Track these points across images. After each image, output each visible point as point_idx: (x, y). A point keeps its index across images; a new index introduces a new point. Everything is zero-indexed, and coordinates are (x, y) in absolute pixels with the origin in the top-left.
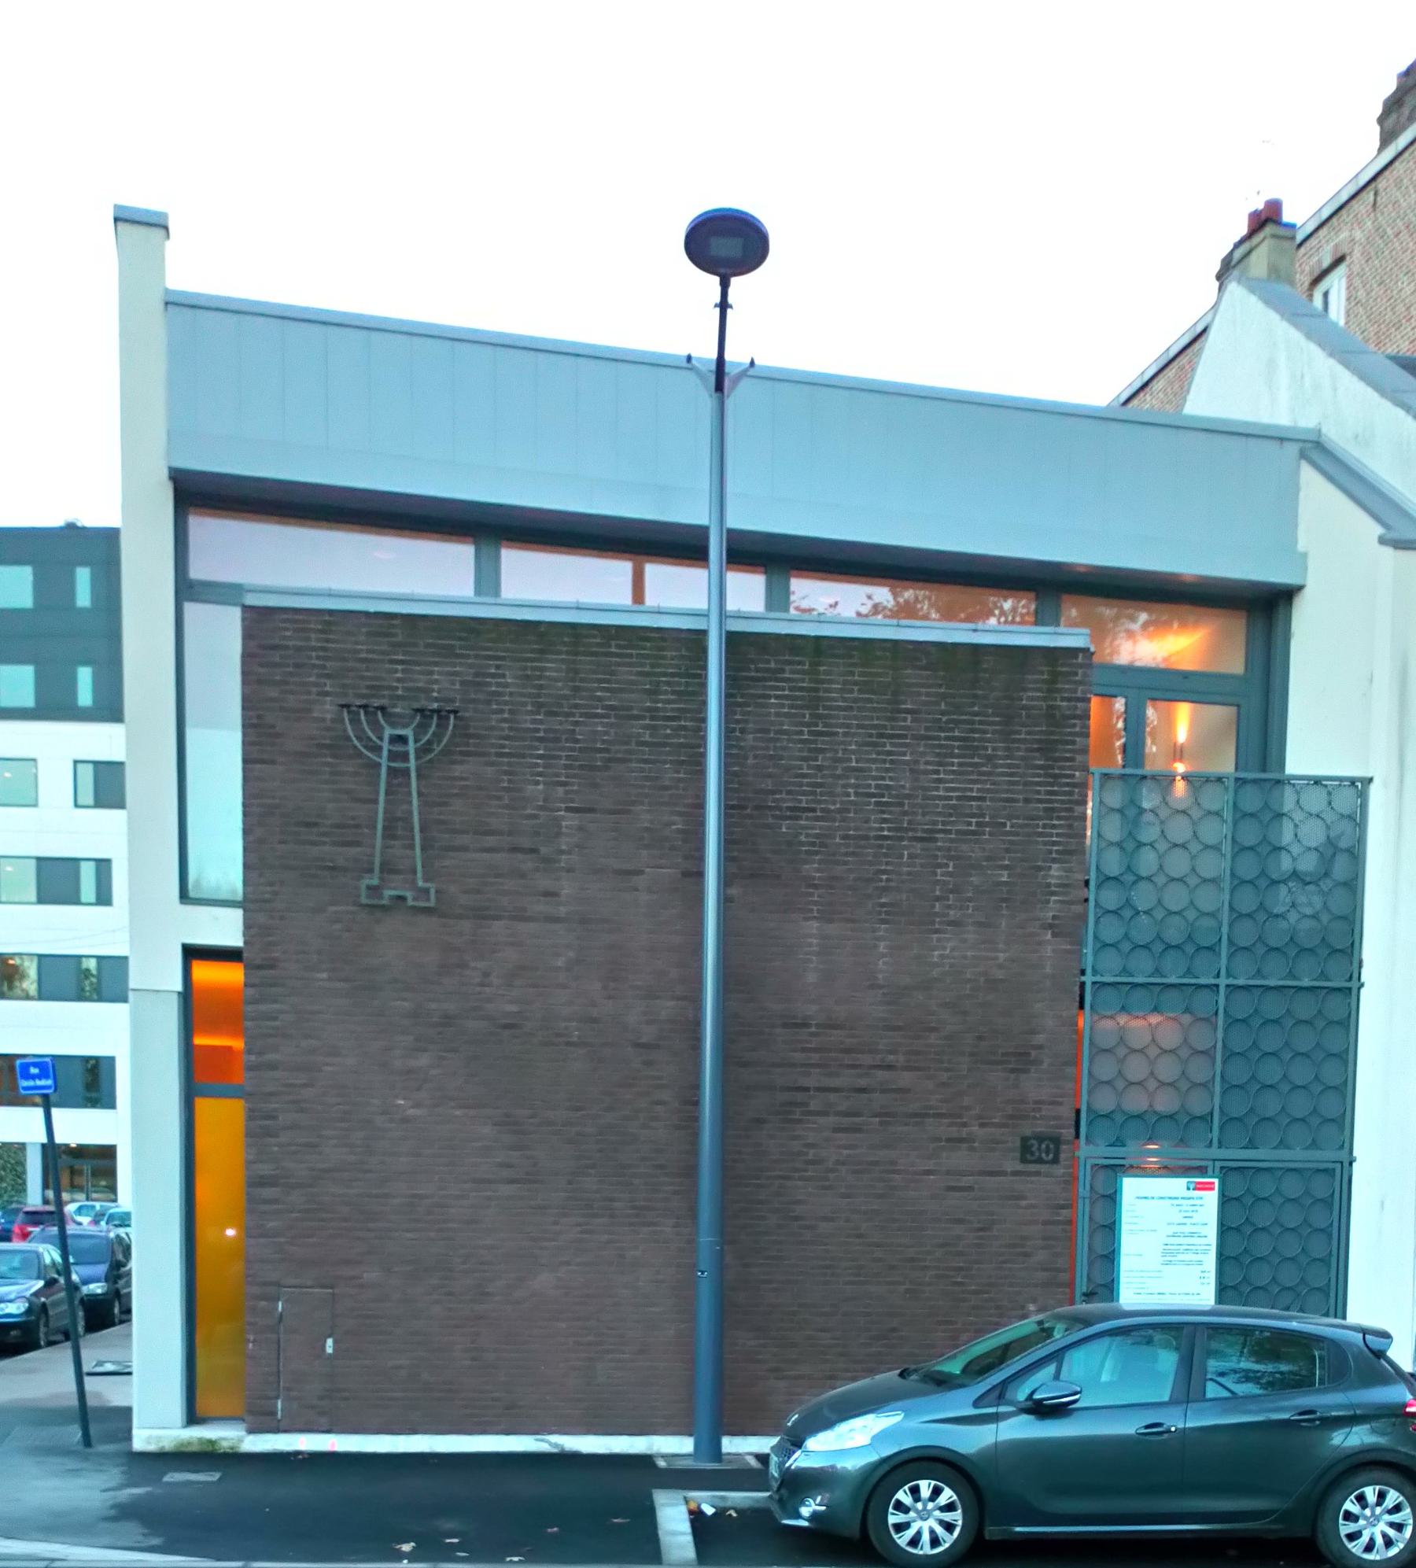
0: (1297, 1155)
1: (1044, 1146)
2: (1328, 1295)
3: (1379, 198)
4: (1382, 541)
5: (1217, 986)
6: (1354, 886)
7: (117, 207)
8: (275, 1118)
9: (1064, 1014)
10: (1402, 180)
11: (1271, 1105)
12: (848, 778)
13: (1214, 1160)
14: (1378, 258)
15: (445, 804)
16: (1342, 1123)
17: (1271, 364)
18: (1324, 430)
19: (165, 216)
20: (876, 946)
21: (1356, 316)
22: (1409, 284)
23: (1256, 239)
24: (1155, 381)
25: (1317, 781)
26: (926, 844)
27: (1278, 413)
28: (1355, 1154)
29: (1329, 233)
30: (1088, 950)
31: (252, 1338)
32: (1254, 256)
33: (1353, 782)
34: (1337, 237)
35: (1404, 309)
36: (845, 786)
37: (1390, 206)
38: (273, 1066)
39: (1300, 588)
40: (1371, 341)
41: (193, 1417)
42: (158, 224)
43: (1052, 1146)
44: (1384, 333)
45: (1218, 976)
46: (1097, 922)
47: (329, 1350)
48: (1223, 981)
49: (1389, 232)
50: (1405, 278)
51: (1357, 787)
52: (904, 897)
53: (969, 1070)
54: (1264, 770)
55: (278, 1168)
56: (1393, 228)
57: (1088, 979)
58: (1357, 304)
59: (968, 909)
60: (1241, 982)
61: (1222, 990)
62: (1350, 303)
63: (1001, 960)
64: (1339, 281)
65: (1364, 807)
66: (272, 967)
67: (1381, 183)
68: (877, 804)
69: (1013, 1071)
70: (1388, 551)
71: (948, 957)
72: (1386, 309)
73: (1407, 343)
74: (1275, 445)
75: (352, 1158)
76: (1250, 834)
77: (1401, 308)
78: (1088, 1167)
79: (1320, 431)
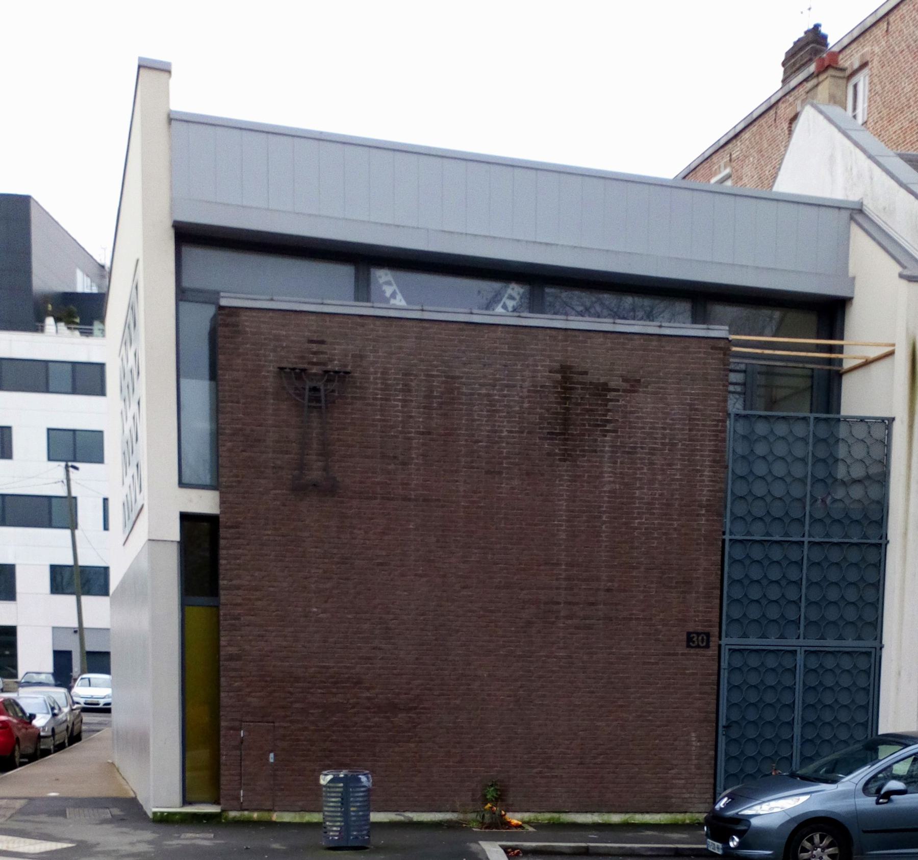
0: (850, 643)
1: (700, 638)
2: (867, 728)
3: (890, 27)
4: (901, 276)
5: (803, 542)
6: (883, 479)
7: (140, 59)
8: (239, 619)
9: (713, 558)
10: (904, 17)
11: (832, 614)
12: (584, 415)
13: (801, 646)
14: (889, 66)
15: (344, 429)
16: (875, 625)
17: (832, 159)
18: (865, 203)
19: (169, 64)
20: (600, 517)
21: (875, 102)
22: (909, 85)
23: (821, 78)
24: (743, 134)
25: (862, 420)
26: (630, 455)
27: (837, 192)
28: (884, 642)
29: (858, 47)
30: (728, 520)
31: (225, 753)
32: (820, 88)
33: (883, 420)
34: (863, 49)
35: (905, 100)
36: (582, 420)
37: (897, 33)
38: (238, 588)
39: (850, 299)
40: (885, 119)
41: (185, 802)
42: (165, 70)
43: (705, 638)
44: (893, 115)
45: (803, 536)
46: (732, 503)
47: (272, 760)
48: (806, 539)
49: (897, 49)
50: (907, 80)
51: (885, 423)
52: (617, 486)
53: (656, 592)
54: (828, 412)
55: (240, 650)
56: (899, 47)
57: (727, 537)
58: (875, 94)
59: (655, 495)
60: (817, 539)
61: (806, 543)
62: (871, 94)
63: (675, 526)
64: (865, 77)
65: (889, 435)
66: (237, 527)
67: (892, 18)
68: (601, 431)
69: (683, 592)
70: (904, 283)
71: (643, 524)
72: (894, 99)
73: (908, 122)
74: (837, 210)
75: (285, 643)
76: (822, 453)
77: (903, 100)
78: (727, 651)
79: (862, 203)
